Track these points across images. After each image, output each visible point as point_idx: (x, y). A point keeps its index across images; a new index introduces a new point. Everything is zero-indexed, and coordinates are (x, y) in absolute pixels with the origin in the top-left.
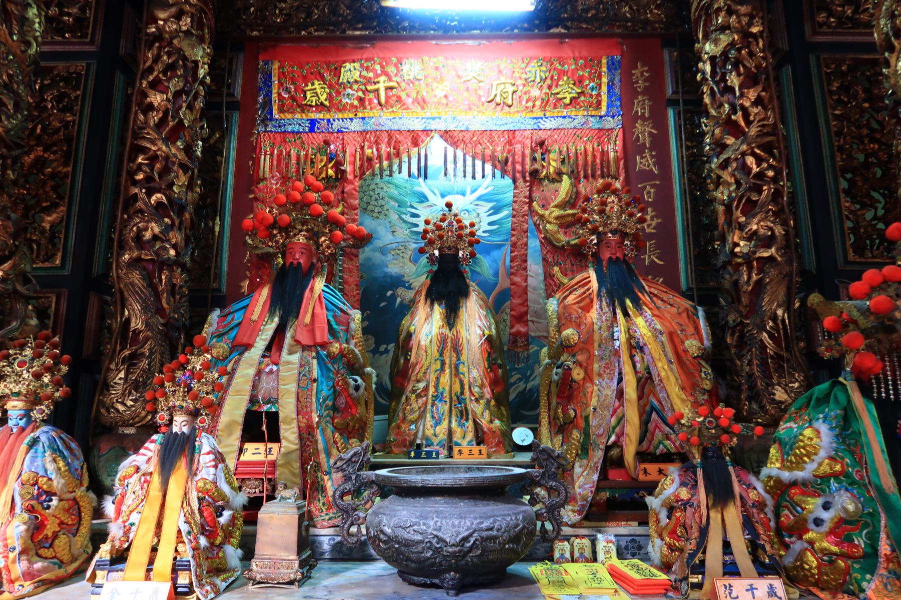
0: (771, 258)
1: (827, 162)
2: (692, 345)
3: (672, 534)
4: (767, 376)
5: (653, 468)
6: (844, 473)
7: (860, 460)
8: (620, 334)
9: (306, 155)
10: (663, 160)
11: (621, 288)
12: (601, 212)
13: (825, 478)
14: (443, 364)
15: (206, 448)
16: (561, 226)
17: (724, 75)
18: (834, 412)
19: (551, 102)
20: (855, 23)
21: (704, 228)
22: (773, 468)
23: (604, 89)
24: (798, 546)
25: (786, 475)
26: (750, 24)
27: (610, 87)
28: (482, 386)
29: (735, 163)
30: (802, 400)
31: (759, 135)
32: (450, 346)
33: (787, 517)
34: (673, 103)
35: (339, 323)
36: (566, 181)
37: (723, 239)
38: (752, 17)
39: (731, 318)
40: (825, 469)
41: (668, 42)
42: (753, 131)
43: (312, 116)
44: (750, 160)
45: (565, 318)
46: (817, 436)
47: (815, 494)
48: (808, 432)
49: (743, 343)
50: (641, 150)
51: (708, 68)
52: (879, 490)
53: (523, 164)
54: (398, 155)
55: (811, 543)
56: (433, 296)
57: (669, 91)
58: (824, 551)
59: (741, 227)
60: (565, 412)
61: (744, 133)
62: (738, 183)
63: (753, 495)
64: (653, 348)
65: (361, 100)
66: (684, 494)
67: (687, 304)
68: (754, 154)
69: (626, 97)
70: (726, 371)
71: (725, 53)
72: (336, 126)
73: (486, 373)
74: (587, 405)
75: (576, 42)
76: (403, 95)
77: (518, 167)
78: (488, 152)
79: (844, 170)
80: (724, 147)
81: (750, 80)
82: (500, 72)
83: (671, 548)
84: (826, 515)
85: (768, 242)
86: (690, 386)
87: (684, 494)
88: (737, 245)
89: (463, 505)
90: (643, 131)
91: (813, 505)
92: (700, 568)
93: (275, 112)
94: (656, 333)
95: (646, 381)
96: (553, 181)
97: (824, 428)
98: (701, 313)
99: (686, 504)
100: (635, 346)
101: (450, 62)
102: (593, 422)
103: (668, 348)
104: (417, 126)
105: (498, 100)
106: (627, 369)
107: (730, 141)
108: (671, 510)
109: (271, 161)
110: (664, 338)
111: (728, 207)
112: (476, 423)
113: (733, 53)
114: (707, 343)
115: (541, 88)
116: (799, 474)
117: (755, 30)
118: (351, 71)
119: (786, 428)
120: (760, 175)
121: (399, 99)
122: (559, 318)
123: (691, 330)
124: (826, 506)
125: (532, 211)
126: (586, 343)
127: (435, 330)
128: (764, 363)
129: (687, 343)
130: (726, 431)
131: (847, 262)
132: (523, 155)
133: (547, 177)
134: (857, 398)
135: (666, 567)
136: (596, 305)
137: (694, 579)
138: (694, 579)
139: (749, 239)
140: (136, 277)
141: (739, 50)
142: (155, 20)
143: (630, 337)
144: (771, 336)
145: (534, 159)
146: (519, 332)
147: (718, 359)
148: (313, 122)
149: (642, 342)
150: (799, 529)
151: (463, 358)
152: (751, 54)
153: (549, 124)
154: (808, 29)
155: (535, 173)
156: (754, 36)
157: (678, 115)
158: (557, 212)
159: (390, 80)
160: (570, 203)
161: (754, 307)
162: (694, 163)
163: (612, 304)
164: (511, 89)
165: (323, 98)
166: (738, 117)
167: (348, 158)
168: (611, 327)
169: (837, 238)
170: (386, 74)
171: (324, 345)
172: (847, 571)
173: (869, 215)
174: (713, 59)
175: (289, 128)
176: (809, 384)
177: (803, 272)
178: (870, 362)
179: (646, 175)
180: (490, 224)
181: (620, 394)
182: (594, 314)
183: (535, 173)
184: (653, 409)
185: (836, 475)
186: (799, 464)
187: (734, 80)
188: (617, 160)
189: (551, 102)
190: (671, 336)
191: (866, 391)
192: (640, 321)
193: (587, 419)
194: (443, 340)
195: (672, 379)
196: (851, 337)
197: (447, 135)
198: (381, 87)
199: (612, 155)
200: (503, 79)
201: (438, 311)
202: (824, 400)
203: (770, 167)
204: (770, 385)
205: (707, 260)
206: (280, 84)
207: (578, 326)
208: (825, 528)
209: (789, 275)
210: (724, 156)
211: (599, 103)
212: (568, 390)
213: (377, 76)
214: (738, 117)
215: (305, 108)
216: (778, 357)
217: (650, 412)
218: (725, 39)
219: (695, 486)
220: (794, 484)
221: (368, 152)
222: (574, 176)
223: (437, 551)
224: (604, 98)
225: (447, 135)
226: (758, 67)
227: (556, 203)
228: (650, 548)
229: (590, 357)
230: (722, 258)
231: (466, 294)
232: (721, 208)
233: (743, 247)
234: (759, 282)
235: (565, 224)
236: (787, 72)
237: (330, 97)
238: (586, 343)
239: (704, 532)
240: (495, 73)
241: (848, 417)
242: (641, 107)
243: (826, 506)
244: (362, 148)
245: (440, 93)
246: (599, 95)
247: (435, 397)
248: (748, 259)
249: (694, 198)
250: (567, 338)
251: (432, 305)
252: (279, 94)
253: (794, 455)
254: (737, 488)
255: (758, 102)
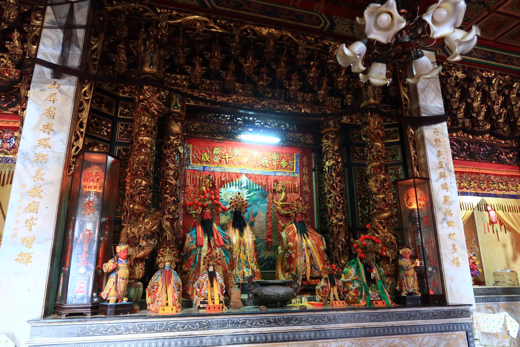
0: (342, 225)
1: (355, 198)
2: (322, 248)
3: (323, 294)
4: (340, 256)
5: (313, 281)
6: (357, 279)
7: (360, 276)
8: (304, 244)
9: (202, 179)
10: (311, 188)
11: (303, 231)
12: (297, 207)
13: (353, 280)
14: (240, 250)
15: (218, 275)
16: (282, 207)
17: (331, 172)
18: (355, 266)
19: (279, 167)
20: (363, 159)
21: (323, 210)
22: (343, 279)
23: (295, 163)
24: (347, 295)
25: (346, 280)
26: (338, 159)
27: (296, 163)
28: (253, 258)
29: (333, 197)
30: (349, 263)
31: (340, 190)
32: (242, 243)
33: (346, 289)
34: (314, 170)
35: (226, 239)
36: (284, 193)
37: (330, 218)
38: (339, 157)
39: (331, 240)
40: (353, 278)
41: (313, 151)
42: (338, 189)
43: (204, 165)
44: (337, 198)
45: (289, 239)
46: (351, 271)
47: (351, 284)
48: (350, 270)
49: (334, 247)
50: (305, 184)
51: (327, 169)
52: (363, 282)
53: (271, 187)
54: (232, 180)
55: (350, 294)
56: (235, 226)
57: (313, 166)
58: (353, 296)
59: (335, 216)
60: (290, 266)
61: (336, 190)
62: (334, 203)
63: (339, 284)
64: (312, 248)
65: (220, 161)
66: (325, 284)
67: (320, 236)
68: (338, 196)
69: (301, 166)
70: (330, 254)
71: (332, 166)
72: (212, 169)
73: (254, 254)
74: (297, 264)
75: (287, 148)
76: (234, 161)
77: (269, 188)
78: (260, 182)
79: (359, 200)
80: (330, 193)
81: (338, 175)
82: (264, 156)
83: (322, 297)
84: (353, 288)
85: (341, 221)
86: (322, 259)
87: (325, 284)
88: (333, 220)
89: (281, 287)
90: (306, 178)
91: (351, 286)
92: (329, 300)
93: (191, 162)
94: (313, 244)
95: (311, 257)
96: (280, 193)
97: (353, 269)
98: (324, 239)
99: (326, 287)
100: (308, 248)
101: (249, 151)
102: (299, 269)
103: (316, 249)
104: (238, 171)
105: (264, 165)
106: (307, 255)
107: (332, 191)
108: (323, 288)
109: (190, 179)
110: (315, 246)
111: (331, 210)
112: (252, 270)
113: (334, 167)
114: (325, 247)
115: (276, 162)
116: (348, 280)
117: (339, 160)
118: (217, 151)
119: (345, 270)
120: (340, 202)
121: (232, 161)
122: (287, 239)
123: (321, 244)
124: (353, 286)
125: (273, 202)
126: (295, 247)
127: (237, 238)
128: (339, 253)
129: (321, 247)
130: (334, 270)
131: (359, 225)
132: (271, 184)
133: (278, 191)
134: (360, 263)
135: (321, 301)
136: (297, 236)
137: (328, 302)
138: (328, 302)
139: (336, 219)
140: (168, 223)
141: (335, 166)
142: (170, 139)
143: (307, 245)
144: (341, 246)
145: (274, 185)
146: (269, 241)
147: (328, 251)
148: (204, 167)
149: (308, 246)
150: (348, 292)
151: (247, 248)
152: (338, 167)
153: (279, 174)
154: (352, 158)
155: (274, 190)
156: (339, 162)
157: (316, 174)
158: (281, 203)
159: (229, 155)
160: (285, 200)
161: (337, 238)
162: (320, 189)
163: (301, 235)
164: (267, 162)
165: (208, 159)
166: (335, 185)
167: (216, 181)
168: (301, 243)
169: (357, 219)
170: (228, 153)
171: (224, 246)
172: (357, 299)
173: (365, 213)
174: (328, 167)
175: (196, 169)
176: (350, 260)
177: (349, 227)
178: (362, 255)
179: (306, 192)
180: (247, 197)
181: (305, 261)
182: (296, 238)
183: (274, 190)
184: (312, 265)
185: (355, 279)
186: (348, 278)
187: (334, 174)
188: (298, 187)
189: (279, 167)
190: (317, 245)
191: (361, 261)
192: (308, 240)
193: (297, 268)
194: (240, 242)
195: (318, 257)
196: (359, 250)
197: (247, 175)
198: (227, 157)
199: (297, 185)
200: (265, 158)
201: (237, 231)
202: (353, 263)
203: (342, 200)
204: (340, 259)
205: (323, 220)
206: (193, 153)
207: (293, 242)
208: (353, 290)
209: (346, 230)
210: (330, 195)
211: (293, 168)
212: (291, 260)
213: (225, 153)
214: (335, 185)
215: (201, 162)
216: (343, 252)
217: (313, 266)
218: (332, 162)
219: (327, 283)
220: (347, 282)
221: (223, 179)
222: (286, 192)
223: (278, 297)
224: (295, 166)
225: (247, 175)
226: (340, 171)
227: (280, 200)
228: (316, 298)
229: (297, 251)
230: (329, 224)
231: (246, 226)
232: (329, 210)
233: (335, 221)
234: (339, 231)
235: (283, 207)
236: (346, 169)
237: (210, 159)
238: (295, 247)
239: (330, 292)
240: (262, 156)
241: (358, 267)
242: (305, 171)
243: (353, 286)
244: (221, 177)
245: (245, 161)
246: (293, 166)
247: (239, 261)
248: (336, 225)
249: (319, 201)
250: (291, 245)
251: (235, 229)
252: (193, 156)
253: (347, 275)
254: (336, 283)
255: (340, 181)
